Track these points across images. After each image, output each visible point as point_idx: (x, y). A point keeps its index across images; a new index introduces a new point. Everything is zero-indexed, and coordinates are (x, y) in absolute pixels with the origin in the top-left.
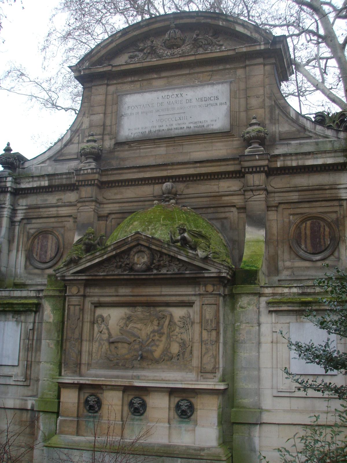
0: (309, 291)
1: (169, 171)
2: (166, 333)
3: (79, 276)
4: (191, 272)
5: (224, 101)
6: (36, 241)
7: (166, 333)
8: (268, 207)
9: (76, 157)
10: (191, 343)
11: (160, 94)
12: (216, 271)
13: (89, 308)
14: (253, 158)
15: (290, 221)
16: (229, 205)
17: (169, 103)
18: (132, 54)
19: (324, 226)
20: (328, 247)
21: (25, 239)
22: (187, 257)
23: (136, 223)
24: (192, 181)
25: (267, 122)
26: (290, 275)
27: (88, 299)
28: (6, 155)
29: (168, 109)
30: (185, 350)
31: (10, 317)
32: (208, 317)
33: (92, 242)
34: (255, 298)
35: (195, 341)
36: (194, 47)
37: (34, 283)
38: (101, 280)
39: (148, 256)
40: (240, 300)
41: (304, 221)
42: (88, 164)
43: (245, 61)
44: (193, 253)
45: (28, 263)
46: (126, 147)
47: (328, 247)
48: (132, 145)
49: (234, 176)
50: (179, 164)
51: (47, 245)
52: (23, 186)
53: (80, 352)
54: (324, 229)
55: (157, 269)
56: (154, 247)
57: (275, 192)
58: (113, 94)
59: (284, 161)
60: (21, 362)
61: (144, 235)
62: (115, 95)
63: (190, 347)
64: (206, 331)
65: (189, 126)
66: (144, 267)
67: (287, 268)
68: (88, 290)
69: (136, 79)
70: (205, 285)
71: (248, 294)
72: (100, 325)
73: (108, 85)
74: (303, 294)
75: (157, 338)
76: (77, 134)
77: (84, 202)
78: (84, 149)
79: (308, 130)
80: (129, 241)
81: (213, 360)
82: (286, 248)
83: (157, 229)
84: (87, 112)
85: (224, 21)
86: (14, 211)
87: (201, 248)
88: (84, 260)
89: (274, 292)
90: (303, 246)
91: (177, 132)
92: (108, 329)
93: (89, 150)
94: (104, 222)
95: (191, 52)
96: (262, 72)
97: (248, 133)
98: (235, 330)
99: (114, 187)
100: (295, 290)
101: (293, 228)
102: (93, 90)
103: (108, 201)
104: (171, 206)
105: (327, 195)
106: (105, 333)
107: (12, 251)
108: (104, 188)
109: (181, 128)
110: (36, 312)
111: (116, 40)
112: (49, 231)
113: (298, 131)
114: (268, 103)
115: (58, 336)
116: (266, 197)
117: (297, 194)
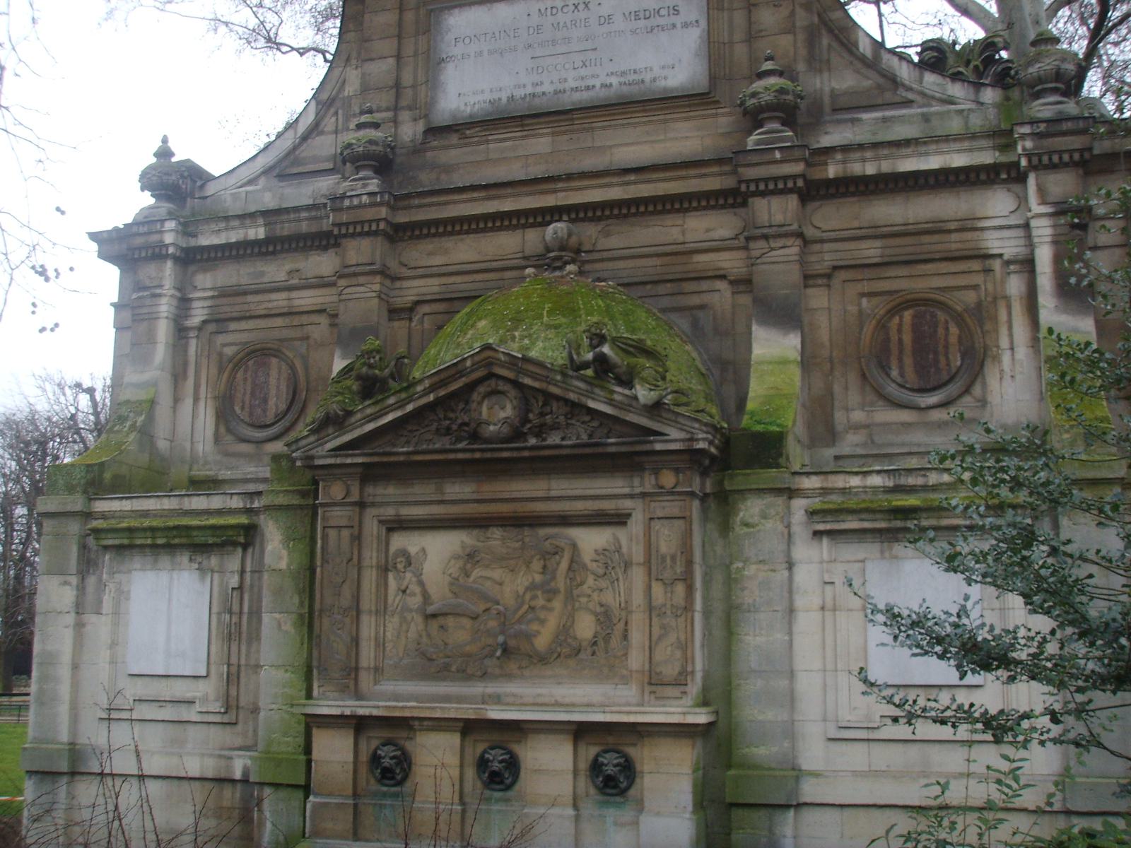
0: (911, 481)
1: (561, 195)
2: (562, 589)
3: (347, 456)
5: (693, 18)
6: (240, 375)
7: (562, 589)
8: (806, 277)
9: (331, 166)
10: (623, 613)
12: (682, 435)
13: (375, 532)
14: (767, 157)
15: (860, 312)
16: (710, 274)
17: (556, 26)
19: (947, 322)
22: (611, 402)
23: (482, 324)
24: (617, 217)
25: (801, 67)
26: (864, 445)
27: (370, 513)
31: (184, 558)
32: (664, 549)
33: (377, 371)
34: (780, 501)
35: (634, 608)
37: (239, 477)
39: (515, 402)
40: (743, 507)
41: (896, 310)
45: (222, 429)
46: (454, 139)
48: (468, 132)
50: (584, 175)
52: (205, 240)
53: (356, 641)
54: (947, 329)
55: (537, 435)
56: (527, 381)
57: (822, 241)
59: (844, 162)
62: (422, 11)
64: (660, 583)
66: (506, 430)
67: (856, 427)
68: (370, 490)
70: (656, 472)
74: (898, 489)
75: (540, 602)
76: (332, 110)
77: (355, 275)
78: (349, 145)
79: (903, 85)
81: (678, 654)
82: (853, 377)
84: (354, 54)
86: (184, 303)
87: (644, 380)
88: (359, 416)
89: (825, 485)
90: (895, 373)
91: (577, 97)
92: (421, 584)
93: (361, 149)
94: (405, 323)
97: (754, 95)
98: (731, 582)
100: (876, 480)
105: (954, 246)
106: (414, 594)
108: (404, 241)
109: (588, 88)
110: (245, 547)
113: (879, 87)
115: (302, 603)
117: (878, 243)
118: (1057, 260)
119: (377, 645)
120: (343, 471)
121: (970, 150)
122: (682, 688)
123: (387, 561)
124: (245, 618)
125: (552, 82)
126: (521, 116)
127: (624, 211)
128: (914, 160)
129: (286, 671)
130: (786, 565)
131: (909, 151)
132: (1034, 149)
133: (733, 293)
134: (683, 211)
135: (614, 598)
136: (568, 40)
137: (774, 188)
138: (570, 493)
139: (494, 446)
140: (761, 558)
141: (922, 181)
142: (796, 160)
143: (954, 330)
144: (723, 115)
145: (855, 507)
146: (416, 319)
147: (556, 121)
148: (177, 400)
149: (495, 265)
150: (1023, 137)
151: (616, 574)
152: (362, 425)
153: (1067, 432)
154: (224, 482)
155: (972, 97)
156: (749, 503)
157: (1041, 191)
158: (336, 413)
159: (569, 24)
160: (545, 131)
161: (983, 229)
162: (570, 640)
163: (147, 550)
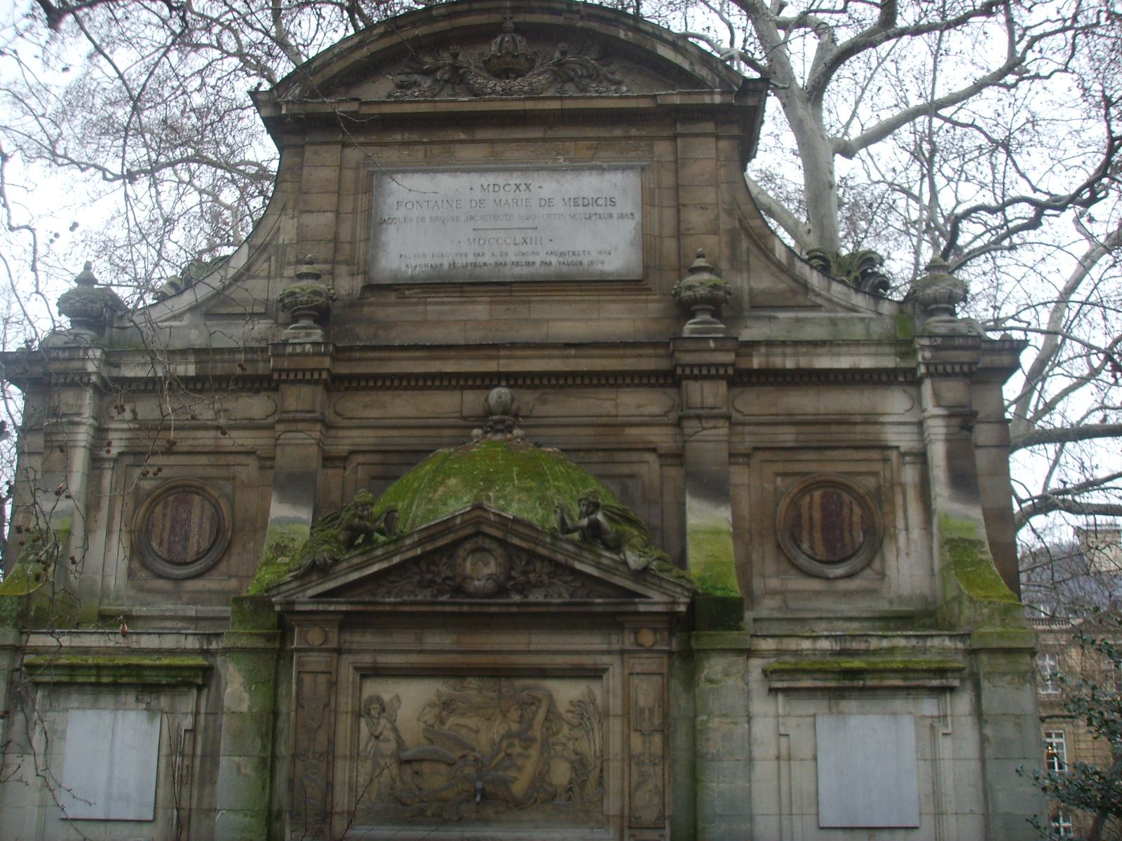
0: (855, 645)
1: (503, 362)
2: (539, 738)
3: (330, 603)
4: (606, 600)
5: (628, 210)
6: (159, 509)
7: (539, 738)
8: (731, 455)
9: (263, 310)
10: (598, 762)
11: (477, 180)
12: (665, 599)
13: (351, 679)
14: (701, 345)
15: (776, 489)
16: (640, 446)
17: (498, 202)
18: (403, 78)
19: (851, 502)
20: (860, 548)
21: (131, 505)
22: (598, 565)
23: (452, 481)
24: (553, 387)
25: (724, 265)
26: (779, 609)
27: (347, 659)
28: (85, 293)
29: (496, 217)
30: (585, 778)
31: (131, 698)
33: (368, 524)
34: (741, 660)
35: (611, 757)
36: (555, 80)
37: (156, 613)
38: (390, 614)
39: (501, 560)
40: (707, 665)
41: (807, 490)
42: (304, 331)
43: (675, 123)
44: (611, 559)
45: (136, 564)
46: (392, 297)
47: (860, 548)
48: (407, 292)
49: (653, 381)
50: (528, 346)
51: (189, 519)
52: (128, 372)
53: (330, 785)
54: (851, 509)
55: (520, 592)
56: (516, 541)
57: (744, 424)
58: (357, 168)
59: (767, 355)
60: (160, 812)
61: (494, 513)
62: (363, 172)
63: (597, 770)
64: (638, 734)
65: (548, 259)
66: (490, 585)
67: (773, 593)
68: (347, 637)
69: (415, 137)
70: (636, 632)
71: (724, 651)
72: (376, 721)
73: (345, 145)
74: (843, 652)
75: (517, 749)
76: (265, 256)
77: (295, 421)
78: (292, 294)
79: (814, 291)
80: (455, 525)
81: (656, 800)
82: (769, 548)
83: (509, 498)
84: (290, 204)
85: (630, 30)
86: (100, 432)
87: (633, 547)
88: (345, 565)
89: (780, 647)
90: (805, 546)
91: (517, 271)
92: (395, 730)
93: (305, 298)
94: (339, 471)
95: (547, 90)
96: (713, 154)
97: (690, 288)
98: (695, 733)
99: (364, 389)
100: (825, 644)
101: (784, 505)
102: (307, 154)
103: (345, 423)
104: (515, 442)
105: (859, 437)
106: (389, 740)
107: (95, 532)
108: (339, 391)
109: (528, 264)
110: (200, 688)
111: (372, 42)
112: (190, 486)
113: (792, 290)
114: (726, 223)
115: (264, 747)
116: (730, 434)
117: (793, 429)
118: (950, 456)
119: (351, 790)
120: (317, 617)
121: (876, 355)
122: (660, 832)
123: (360, 707)
124: (197, 762)
125: (493, 254)
126: (462, 284)
127: (562, 382)
128: (828, 359)
129: (246, 815)
130: (746, 719)
131: (824, 350)
132: (932, 358)
133: (661, 466)
134: (616, 386)
135: (590, 746)
136: (509, 217)
137: (706, 373)
138: (550, 647)
139: (480, 601)
140: (724, 712)
141: (832, 378)
142: (728, 351)
143: (857, 510)
144: (653, 301)
145: (810, 667)
146: (349, 468)
147: (495, 291)
148: (88, 532)
149: (431, 422)
150: (923, 347)
151: (591, 724)
152: (346, 574)
153: (986, 607)
154: (139, 618)
155: (872, 307)
156: (713, 661)
157: (937, 396)
158: (325, 560)
159: (510, 202)
160: (483, 299)
161: (883, 424)
162: (546, 786)
163: (88, 688)
